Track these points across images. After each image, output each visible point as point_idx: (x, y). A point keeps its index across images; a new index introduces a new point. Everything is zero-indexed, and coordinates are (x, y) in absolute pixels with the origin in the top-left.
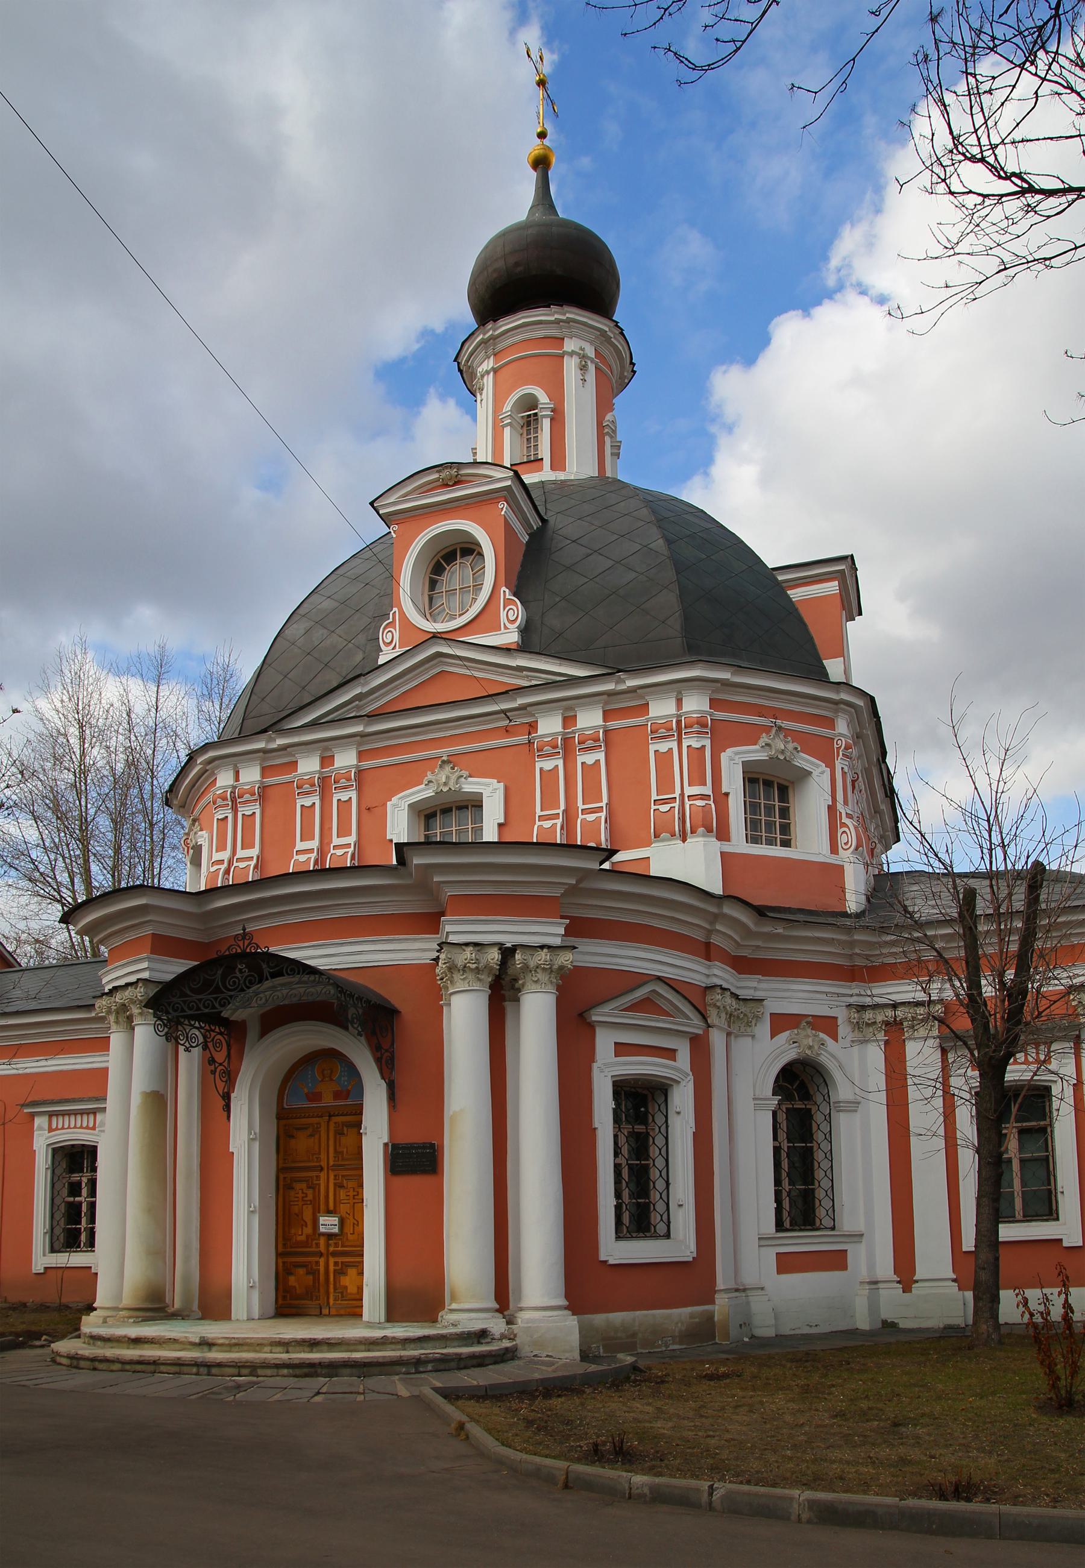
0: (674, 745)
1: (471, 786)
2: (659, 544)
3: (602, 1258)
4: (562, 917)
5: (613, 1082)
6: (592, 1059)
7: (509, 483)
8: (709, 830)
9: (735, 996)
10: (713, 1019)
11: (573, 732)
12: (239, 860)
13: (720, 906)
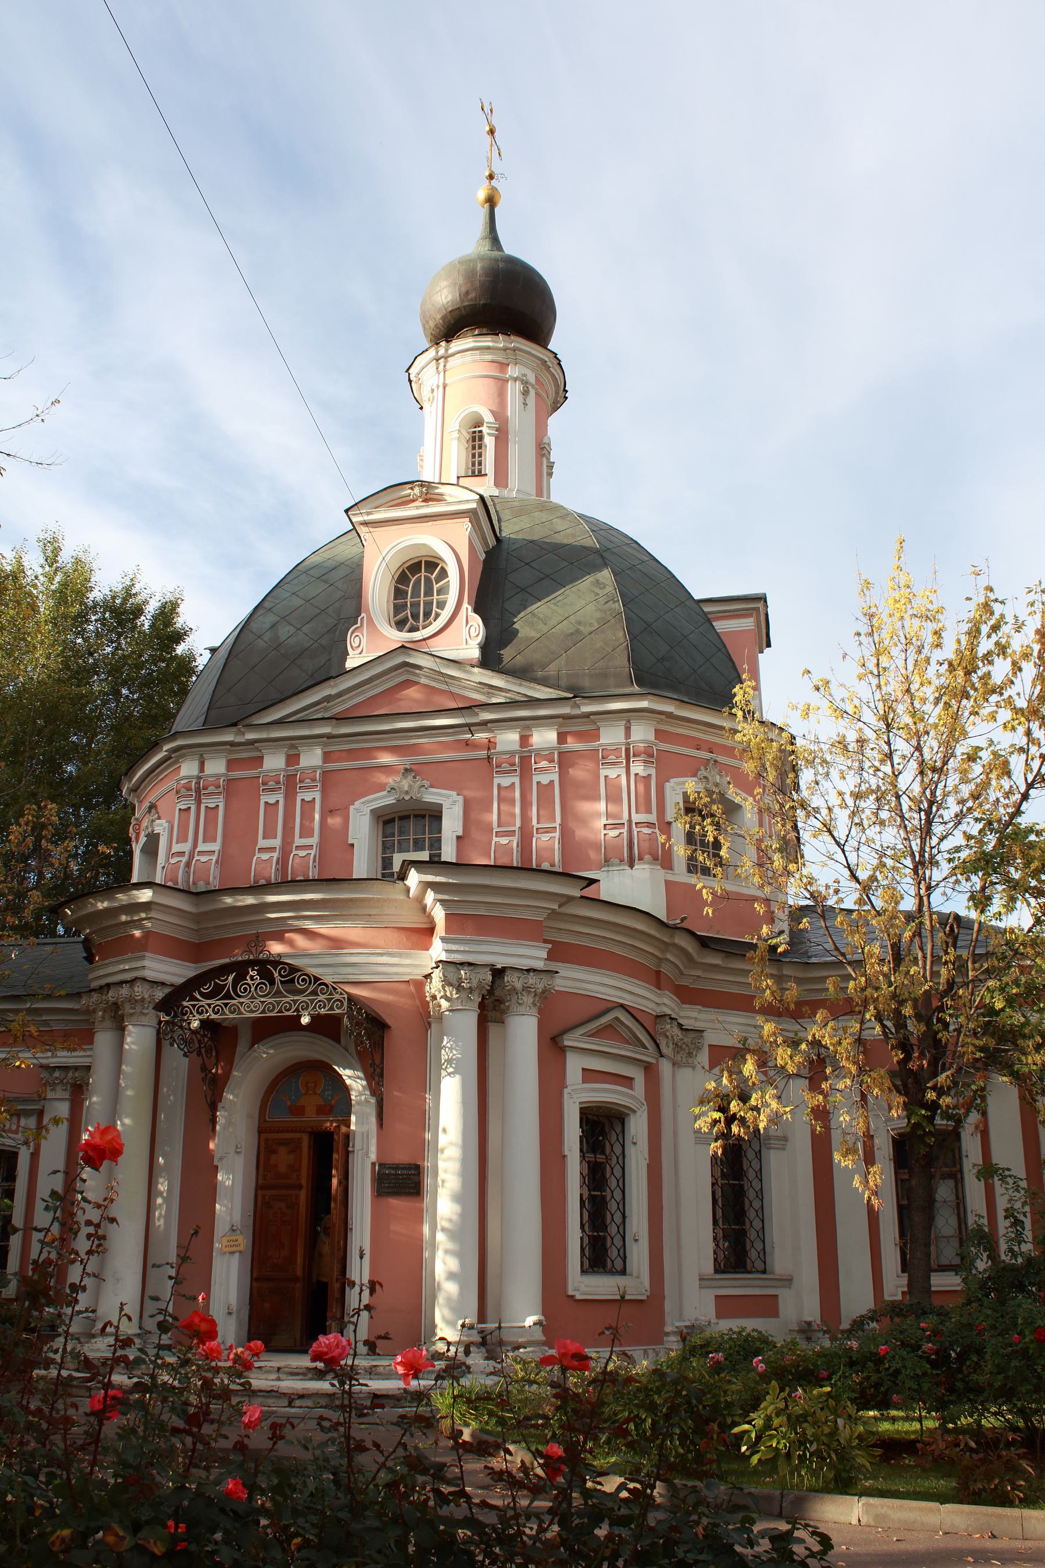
0: (623, 772)
1: (432, 796)
3: (570, 1293)
4: (545, 941)
5: (581, 1109)
7: (474, 505)
8: (655, 858)
9: (680, 1025)
11: (529, 751)
12: (201, 853)
13: (672, 936)
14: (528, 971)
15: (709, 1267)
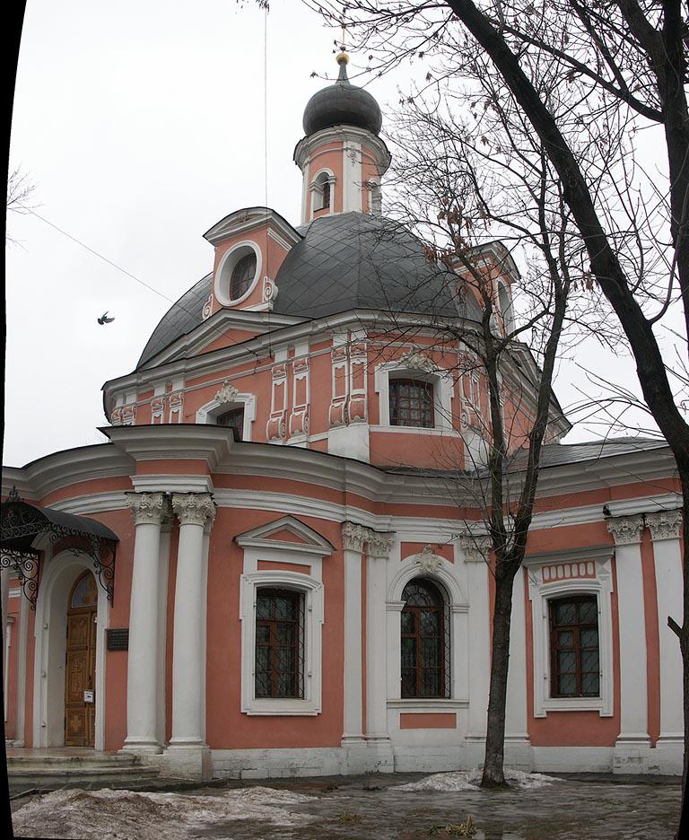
0: (346, 363)
3: (242, 711)
12: (353, 396)
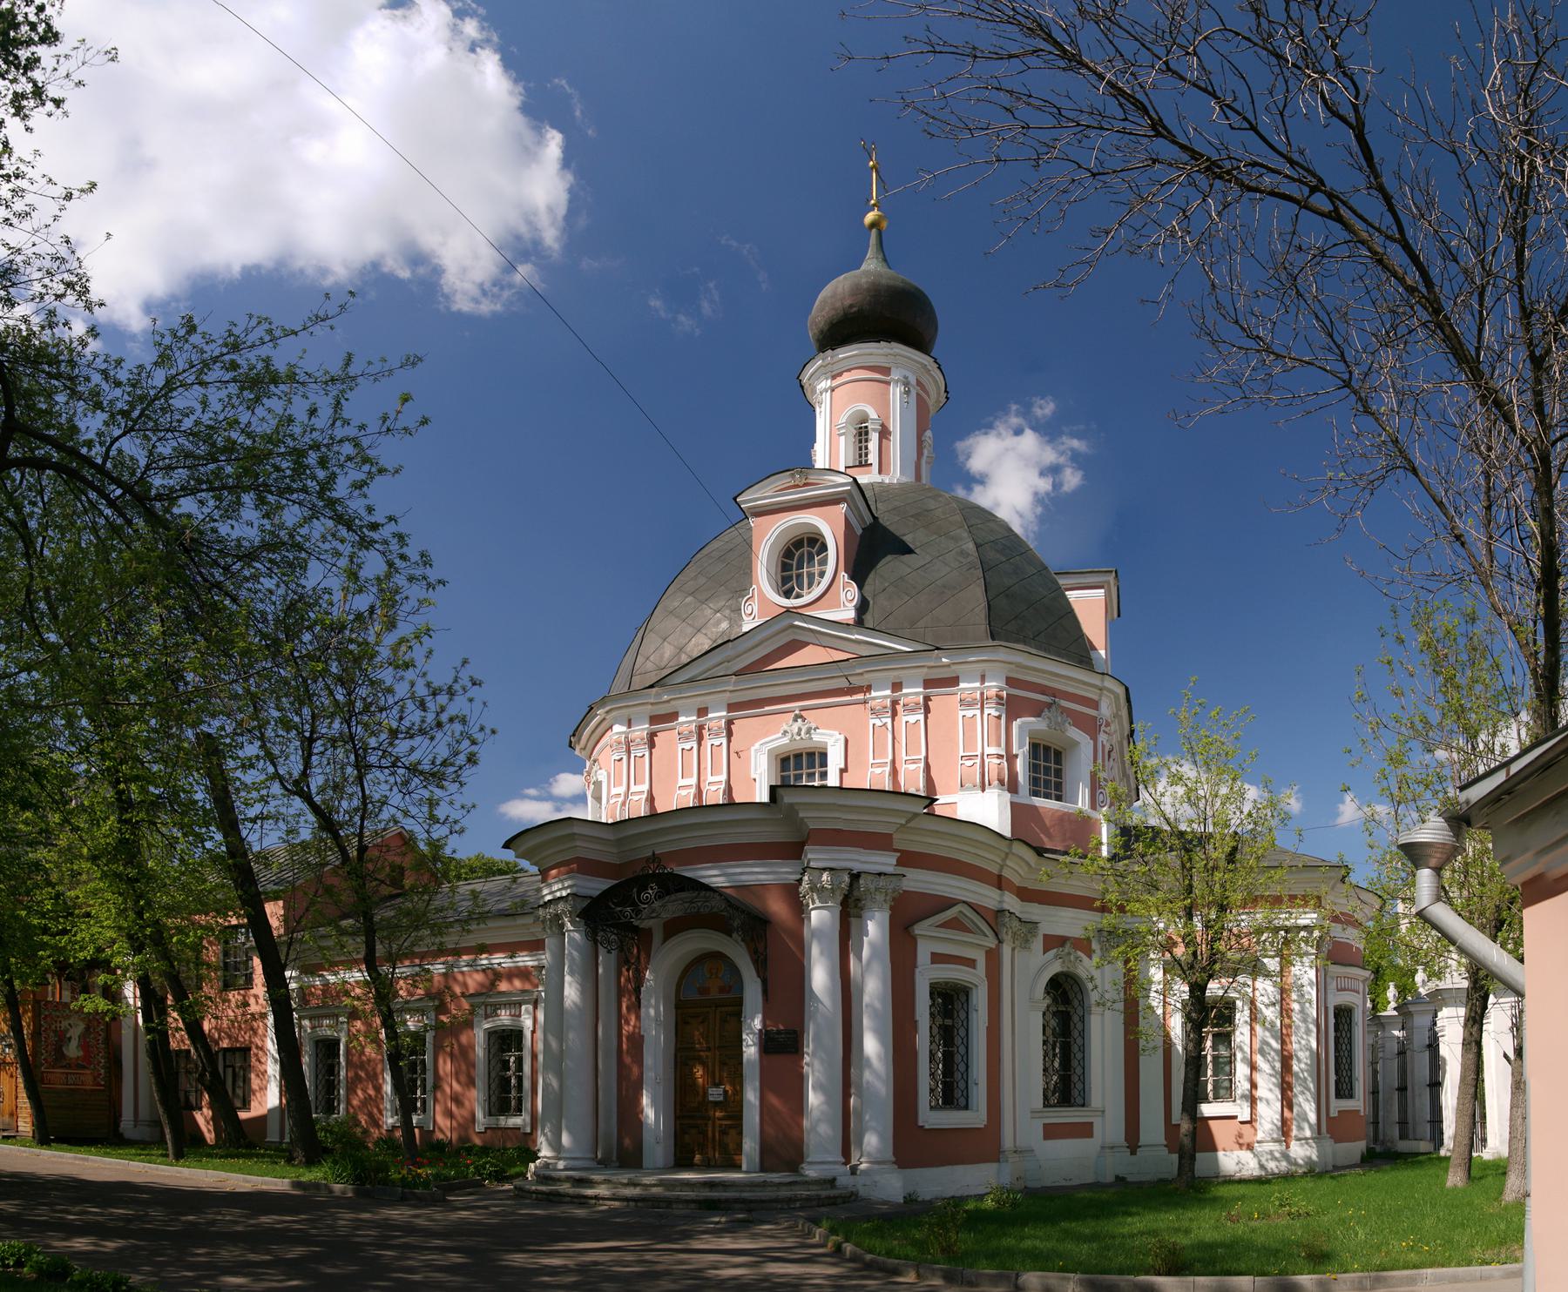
0: (978, 712)
2: (971, 546)
3: (920, 1124)
6: (914, 966)
10: (1003, 936)
12: (634, 793)
14: (880, 874)
15: (1038, 1102)
